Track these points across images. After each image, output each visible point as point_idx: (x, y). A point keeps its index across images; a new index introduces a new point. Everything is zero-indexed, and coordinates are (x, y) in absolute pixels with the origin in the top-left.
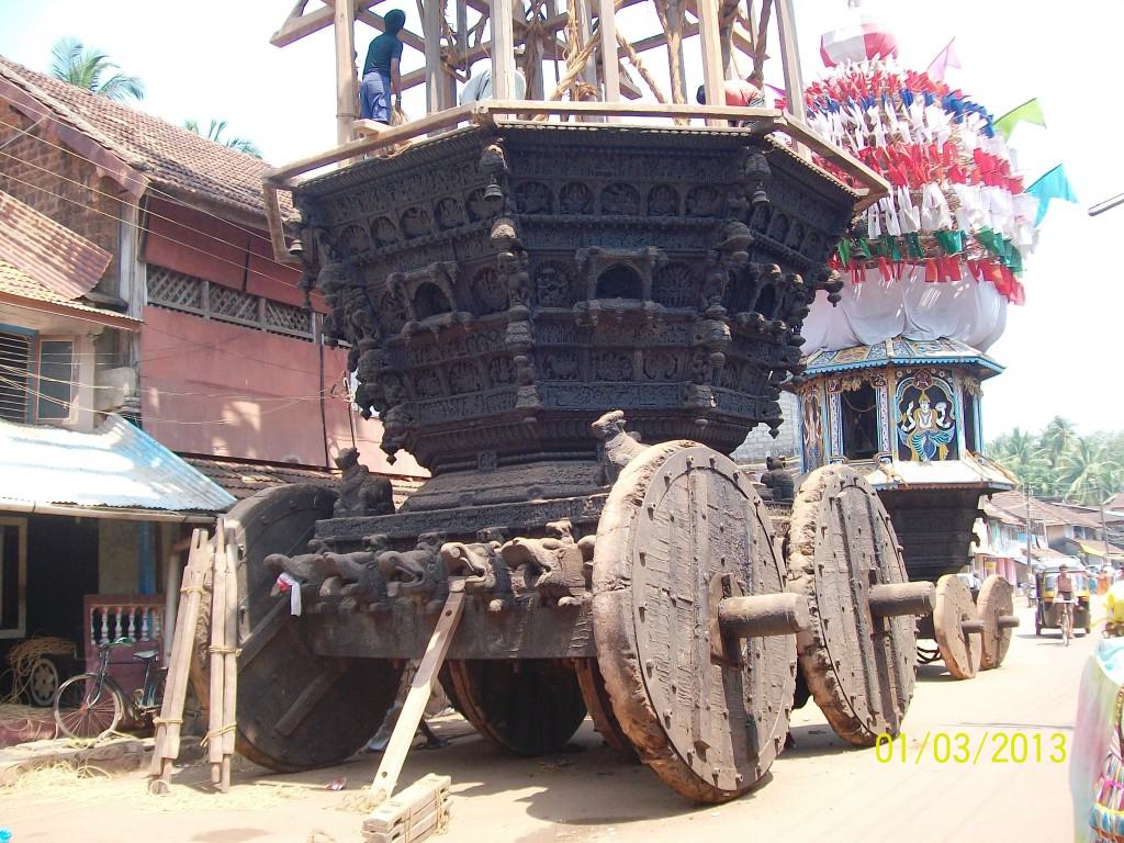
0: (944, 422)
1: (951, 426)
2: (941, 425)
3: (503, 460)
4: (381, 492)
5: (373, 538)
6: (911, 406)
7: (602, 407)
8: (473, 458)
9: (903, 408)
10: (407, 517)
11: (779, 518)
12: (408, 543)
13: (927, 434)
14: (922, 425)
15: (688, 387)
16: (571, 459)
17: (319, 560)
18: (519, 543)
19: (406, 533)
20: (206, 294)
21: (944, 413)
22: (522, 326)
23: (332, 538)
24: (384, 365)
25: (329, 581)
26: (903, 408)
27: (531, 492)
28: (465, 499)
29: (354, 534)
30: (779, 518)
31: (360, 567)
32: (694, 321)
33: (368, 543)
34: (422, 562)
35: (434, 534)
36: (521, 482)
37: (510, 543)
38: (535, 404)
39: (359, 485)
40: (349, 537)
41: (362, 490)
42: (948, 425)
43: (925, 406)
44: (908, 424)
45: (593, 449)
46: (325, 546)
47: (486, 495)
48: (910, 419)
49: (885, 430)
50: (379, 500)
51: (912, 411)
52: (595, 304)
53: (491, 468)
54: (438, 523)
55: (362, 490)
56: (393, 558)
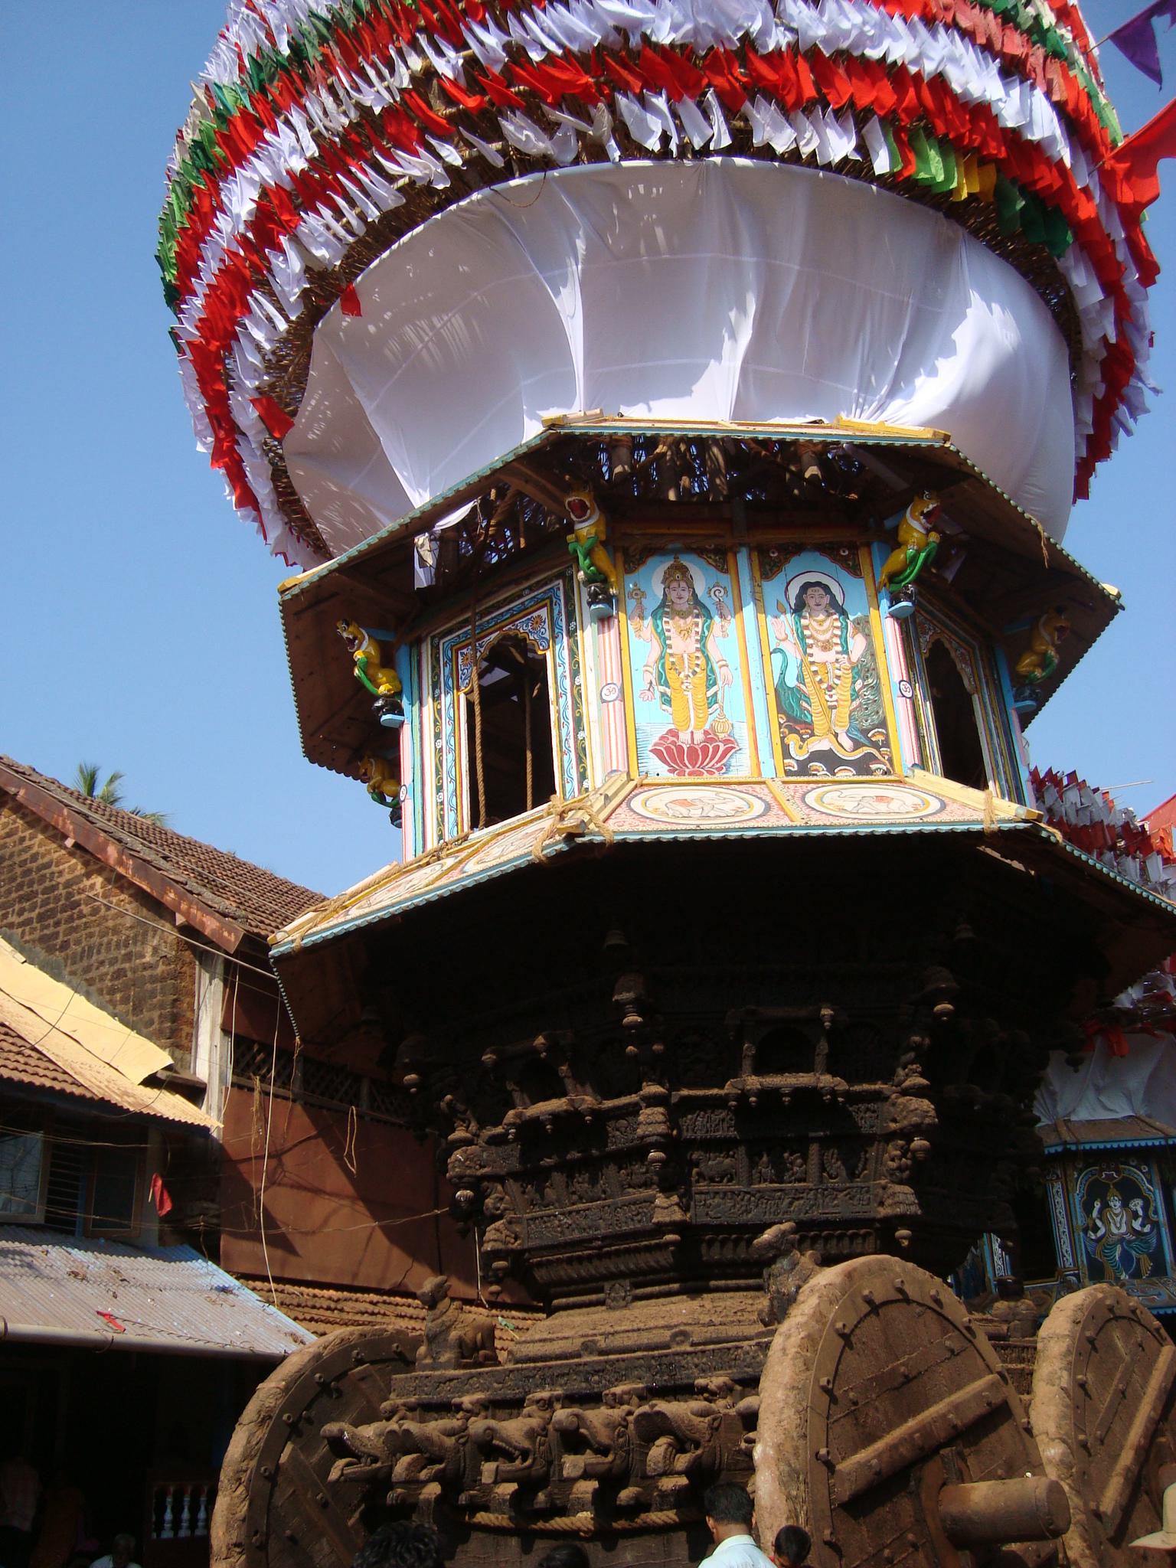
0: (1143, 1225)
1: (1152, 1230)
2: (1138, 1228)
3: (640, 1291)
4: (479, 1336)
5: (467, 1400)
6: (1097, 1205)
7: (767, 1218)
8: (601, 1290)
9: (1088, 1208)
10: (511, 1371)
11: (1020, 1366)
12: (513, 1405)
13: (1121, 1240)
14: (1114, 1230)
15: (884, 1188)
16: (738, 1289)
17: (392, 1432)
18: (657, 1409)
19: (509, 1394)
20: (365, 1090)
21: (1141, 1213)
22: (657, 1113)
23: (413, 1399)
24: (482, 1167)
25: (406, 1460)
26: (1088, 1208)
27: (675, 1335)
28: (588, 1347)
29: (443, 1394)
30: (1020, 1366)
31: (450, 1442)
32: (887, 1098)
33: (459, 1407)
34: (531, 1434)
35: (545, 1394)
36: (662, 1323)
37: (645, 1408)
38: (678, 1216)
39: (449, 1327)
40: (435, 1398)
41: (454, 1334)
42: (1147, 1229)
43: (1116, 1204)
44: (1096, 1229)
45: (760, 1275)
46: (402, 1411)
47: (618, 1341)
48: (1099, 1223)
49: (1065, 1238)
50: (476, 1348)
51: (1100, 1212)
52: (753, 1082)
53: (623, 1303)
54: (550, 1378)
55: (454, 1334)
56: (489, 1428)
